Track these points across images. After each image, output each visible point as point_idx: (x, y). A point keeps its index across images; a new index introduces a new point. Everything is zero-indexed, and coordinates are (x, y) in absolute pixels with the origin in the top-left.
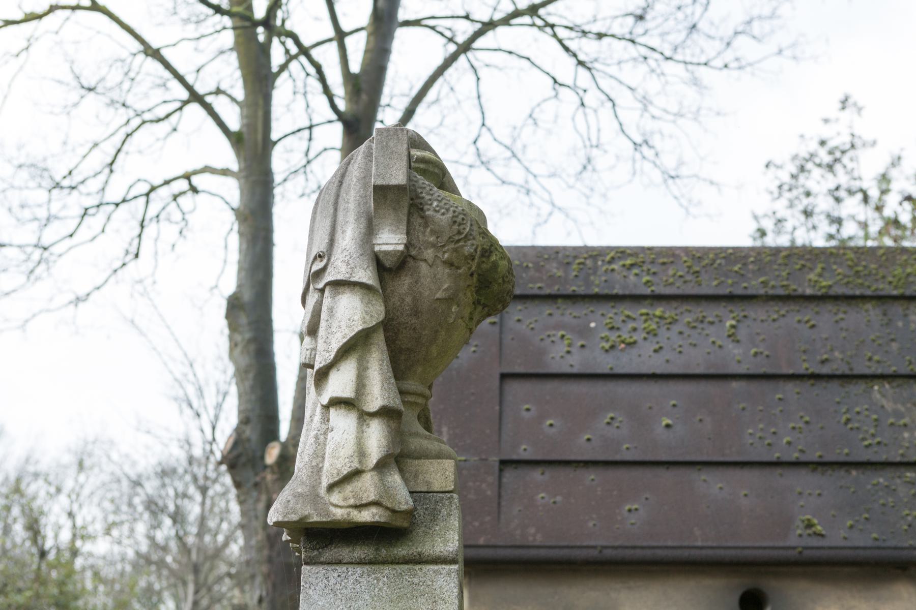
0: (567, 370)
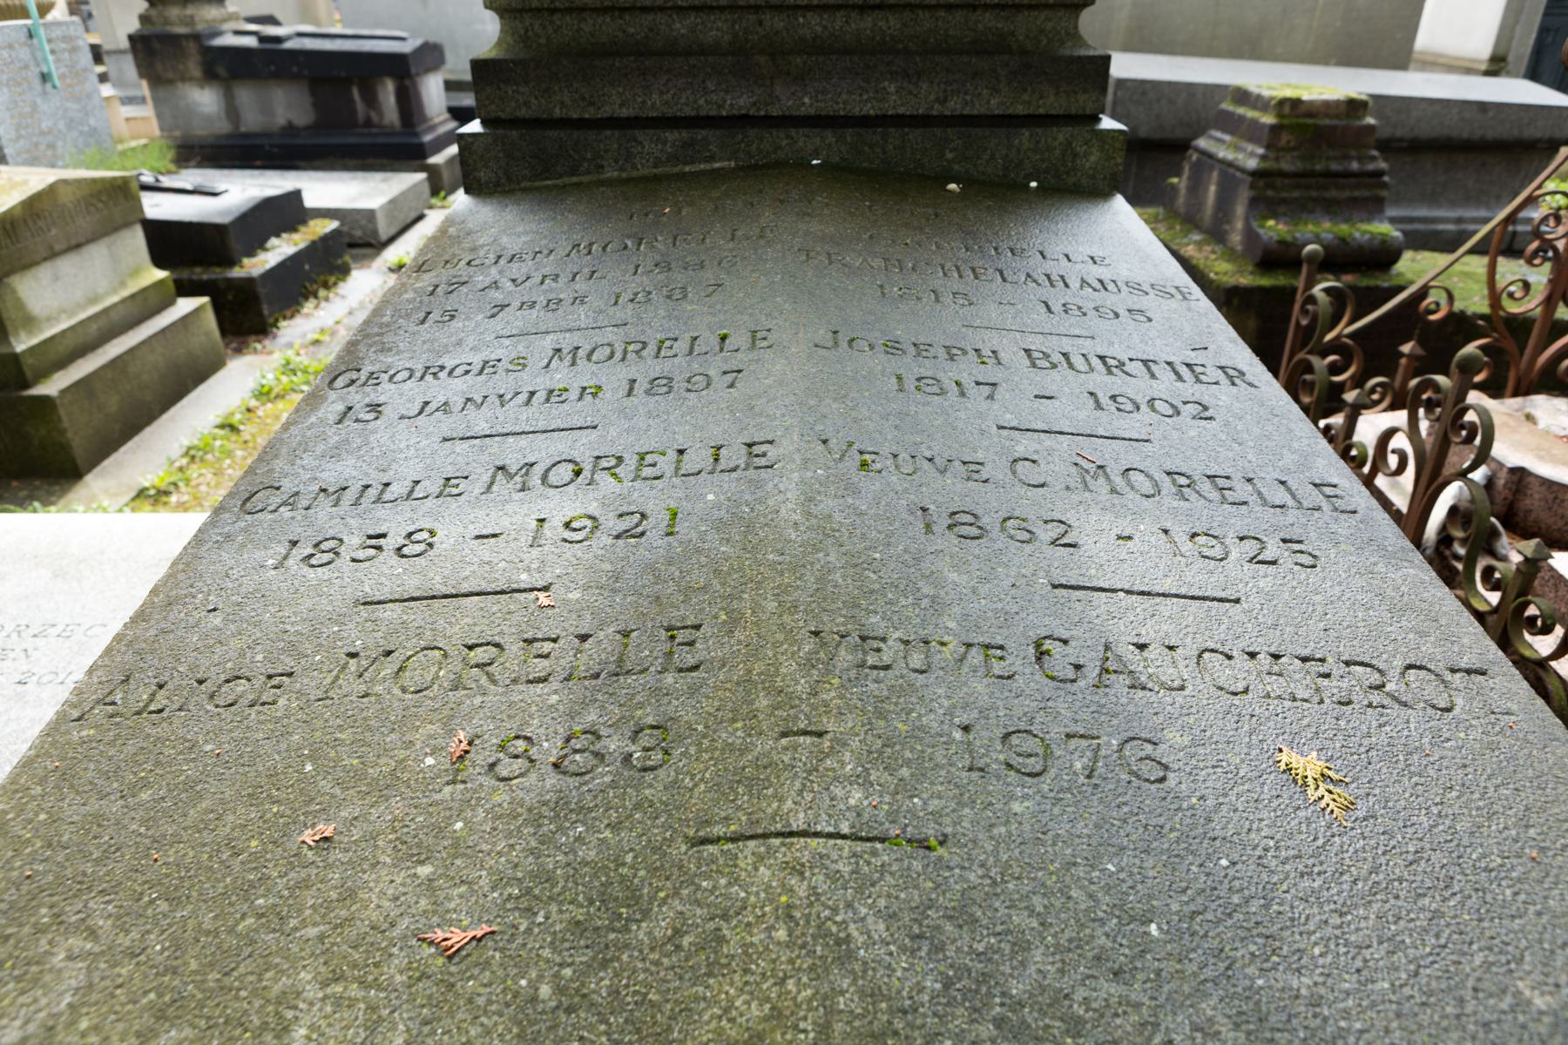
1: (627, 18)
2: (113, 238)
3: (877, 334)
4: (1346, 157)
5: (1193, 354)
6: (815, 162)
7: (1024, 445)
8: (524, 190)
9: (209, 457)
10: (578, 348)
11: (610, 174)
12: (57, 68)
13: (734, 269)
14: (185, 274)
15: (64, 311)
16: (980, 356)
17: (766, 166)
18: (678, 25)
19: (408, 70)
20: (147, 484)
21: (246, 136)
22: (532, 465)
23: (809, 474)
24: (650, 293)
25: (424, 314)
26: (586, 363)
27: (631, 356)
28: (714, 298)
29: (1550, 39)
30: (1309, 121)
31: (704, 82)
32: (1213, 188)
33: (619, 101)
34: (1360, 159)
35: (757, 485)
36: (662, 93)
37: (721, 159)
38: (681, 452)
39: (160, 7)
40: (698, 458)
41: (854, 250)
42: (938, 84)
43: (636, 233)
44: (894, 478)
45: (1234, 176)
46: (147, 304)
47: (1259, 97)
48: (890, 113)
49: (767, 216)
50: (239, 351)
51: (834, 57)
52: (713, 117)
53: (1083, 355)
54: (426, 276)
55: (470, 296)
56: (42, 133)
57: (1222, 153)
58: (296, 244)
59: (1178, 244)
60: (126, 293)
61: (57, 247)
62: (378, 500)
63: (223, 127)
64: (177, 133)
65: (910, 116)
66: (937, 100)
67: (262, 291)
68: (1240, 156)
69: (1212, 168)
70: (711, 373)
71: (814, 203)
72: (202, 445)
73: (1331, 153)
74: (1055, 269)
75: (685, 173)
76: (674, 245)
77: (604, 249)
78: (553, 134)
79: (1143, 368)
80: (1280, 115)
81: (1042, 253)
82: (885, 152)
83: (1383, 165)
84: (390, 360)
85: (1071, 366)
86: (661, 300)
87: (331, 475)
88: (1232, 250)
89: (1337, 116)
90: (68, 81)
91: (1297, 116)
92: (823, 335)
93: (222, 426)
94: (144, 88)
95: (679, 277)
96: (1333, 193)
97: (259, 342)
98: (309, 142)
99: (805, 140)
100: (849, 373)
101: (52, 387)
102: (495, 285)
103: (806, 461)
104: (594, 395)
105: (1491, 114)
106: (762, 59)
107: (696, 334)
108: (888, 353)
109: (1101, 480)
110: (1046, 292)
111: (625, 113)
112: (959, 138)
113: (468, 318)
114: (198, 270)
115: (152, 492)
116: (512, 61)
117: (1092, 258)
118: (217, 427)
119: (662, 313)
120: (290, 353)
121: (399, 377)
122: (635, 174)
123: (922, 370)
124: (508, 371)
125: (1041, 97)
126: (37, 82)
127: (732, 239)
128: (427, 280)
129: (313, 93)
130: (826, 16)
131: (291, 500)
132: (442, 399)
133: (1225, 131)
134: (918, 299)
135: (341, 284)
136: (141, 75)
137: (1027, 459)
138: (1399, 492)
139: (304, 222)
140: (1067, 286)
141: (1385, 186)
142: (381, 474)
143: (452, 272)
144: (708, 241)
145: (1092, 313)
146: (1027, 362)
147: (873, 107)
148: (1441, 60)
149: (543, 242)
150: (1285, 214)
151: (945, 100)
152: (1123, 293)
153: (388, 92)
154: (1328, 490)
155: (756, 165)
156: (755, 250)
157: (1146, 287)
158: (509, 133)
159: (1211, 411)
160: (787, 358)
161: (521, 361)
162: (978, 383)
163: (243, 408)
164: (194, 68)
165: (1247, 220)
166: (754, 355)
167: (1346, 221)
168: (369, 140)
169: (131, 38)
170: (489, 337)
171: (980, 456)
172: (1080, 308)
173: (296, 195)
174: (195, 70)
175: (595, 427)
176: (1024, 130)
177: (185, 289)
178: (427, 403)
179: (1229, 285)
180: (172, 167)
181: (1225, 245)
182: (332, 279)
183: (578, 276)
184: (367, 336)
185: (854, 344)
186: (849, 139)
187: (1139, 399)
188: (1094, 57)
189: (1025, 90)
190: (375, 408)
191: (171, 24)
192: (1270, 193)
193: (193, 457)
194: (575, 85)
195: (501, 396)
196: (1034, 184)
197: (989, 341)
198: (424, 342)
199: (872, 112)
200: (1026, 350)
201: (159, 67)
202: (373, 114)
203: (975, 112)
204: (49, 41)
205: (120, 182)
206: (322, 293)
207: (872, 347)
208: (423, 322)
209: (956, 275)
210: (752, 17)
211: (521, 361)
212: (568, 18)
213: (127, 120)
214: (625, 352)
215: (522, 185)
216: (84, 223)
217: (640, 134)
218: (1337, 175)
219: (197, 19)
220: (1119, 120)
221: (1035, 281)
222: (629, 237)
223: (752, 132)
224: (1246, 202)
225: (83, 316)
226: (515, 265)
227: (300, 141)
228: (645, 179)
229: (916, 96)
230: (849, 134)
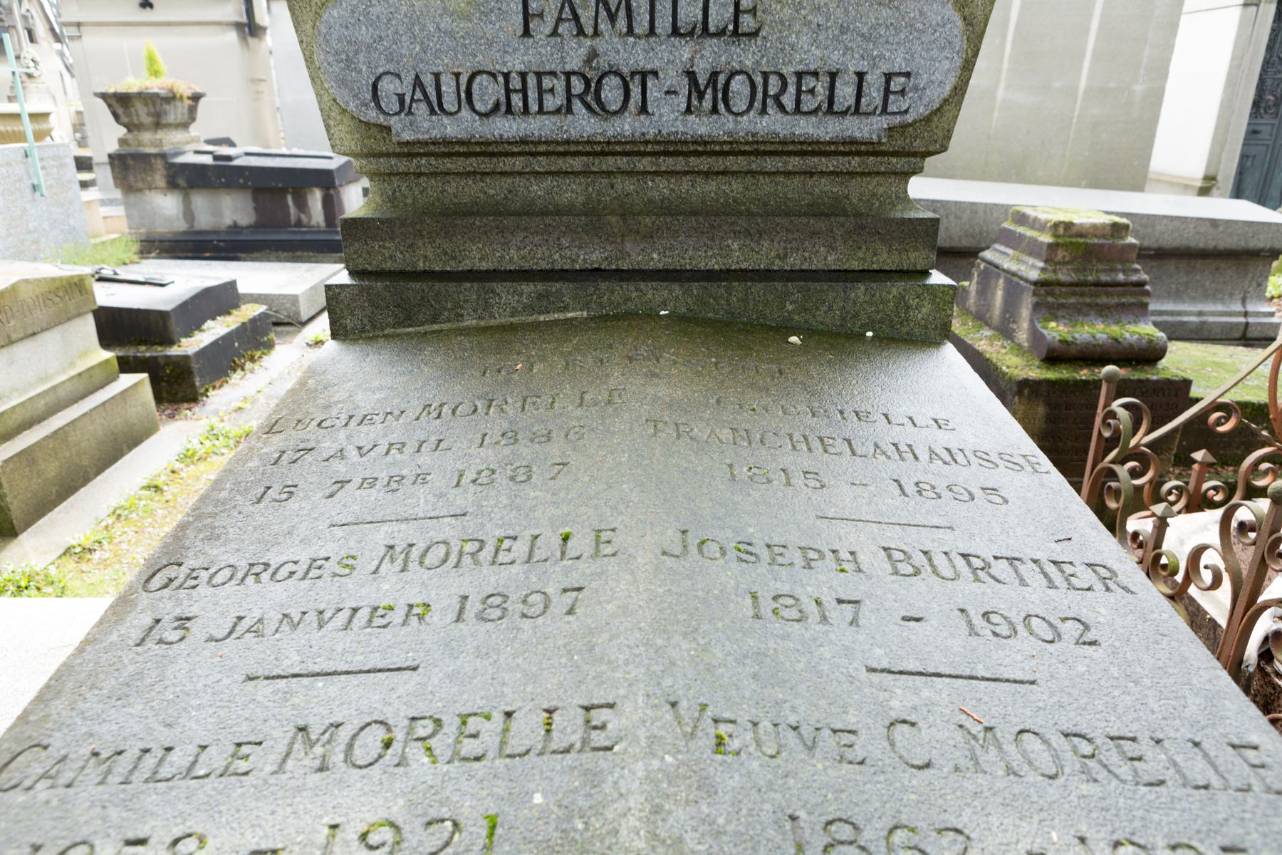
1: (488, 181)
2: (66, 326)
3: (729, 533)
4: (1113, 270)
5: (1058, 547)
6: (662, 313)
7: (902, 695)
8: (386, 337)
9: (134, 516)
10: (411, 545)
11: (470, 322)
12: (45, 181)
13: (581, 443)
14: (130, 352)
15: (17, 390)
16: (838, 560)
17: (616, 317)
18: (535, 188)
19: (334, 182)
20: (74, 543)
21: (199, 233)
22: (338, 726)
23: (656, 764)
24: (493, 472)
25: (263, 489)
26: (418, 568)
27: (467, 560)
28: (559, 482)
29: (1249, 163)
30: (1081, 240)
31: (558, 239)
32: (999, 294)
33: (479, 256)
34: (1124, 272)
35: (593, 778)
36: (519, 248)
37: (574, 310)
38: (509, 715)
39: (136, 133)
40: (527, 730)
41: (701, 419)
42: (779, 243)
43: (487, 394)
44: (755, 764)
45: (1019, 284)
46: (92, 382)
47: (1035, 219)
48: (733, 268)
49: (616, 377)
50: (172, 417)
51: (681, 218)
52: (567, 270)
53: (946, 553)
54: (276, 439)
55: (314, 468)
56: (29, 232)
57: (1007, 264)
58: (228, 326)
59: (972, 339)
60: (74, 372)
61: (14, 336)
62: (154, 778)
63: (181, 226)
64: (143, 230)
65: (752, 271)
66: (778, 256)
67: (195, 366)
68: (1023, 268)
69: (998, 276)
70: (550, 590)
71: (662, 360)
72: (127, 505)
73: (1100, 267)
74: (904, 435)
75: (540, 322)
76: (523, 409)
77: (454, 412)
78: (416, 286)
79: (1010, 570)
80: (1056, 236)
81: (886, 416)
82: (729, 305)
83: (1145, 277)
84: (215, 552)
85: (935, 571)
86: (504, 482)
87: (107, 736)
88: (1020, 345)
89: (1104, 236)
90: (54, 190)
91: (1070, 236)
92: (671, 537)
93: (148, 487)
94: (118, 194)
95: (525, 451)
96: (1104, 300)
97: (190, 409)
98: (250, 238)
99: (653, 293)
100: (700, 593)
101: (290, 199)
102: (341, 455)
103: (652, 739)
104: (421, 617)
105: (1221, 229)
106: (613, 219)
107: (537, 532)
108: (742, 560)
109: (993, 751)
110: (895, 467)
111: (484, 266)
112: (798, 292)
113: (306, 498)
114: (143, 348)
115: (78, 550)
116: (379, 220)
117: (936, 421)
118: (144, 488)
119: (504, 500)
120: (215, 420)
121: (219, 579)
122: (492, 322)
123: (779, 585)
124: (335, 575)
125: (875, 254)
126: (28, 191)
127: (581, 405)
128: (277, 441)
129: (255, 200)
130: (673, 181)
131: (53, 772)
132: (257, 614)
133: (1007, 245)
134: (769, 481)
135: (265, 357)
136: (117, 185)
137: (904, 722)
138: (1218, 605)
139: (237, 306)
140: (916, 458)
141: (1147, 294)
142: (166, 731)
143: (302, 435)
144: (556, 405)
145: (946, 494)
146: (888, 567)
147: (717, 263)
148: (1163, 178)
149: (397, 401)
150: (1064, 317)
151: (785, 256)
152: (973, 466)
153: (316, 199)
154: (1251, 754)
155: (607, 315)
156: (603, 418)
157: (994, 458)
158: (373, 284)
159: (1093, 631)
160: (632, 573)
161: (350, 562)
162: (840, 601)
163: (168, 470)
164: (159, 179)
165: (1032, 321)
166: (595, 566)
167: (1117, 323)
168: (299, 237)
169: (110, 156)
170: (323, 525)
171: (851, 720)
172: (933, 487)
173: (232, 284)
174: (161, 182)
175: (415, 669)
176: (860, 285)
177: (126, 366)
178: (240, 618)
179: (1020, 378)
180: (136, 258)
181: (1013, 341)
182: (258, 354)
183: (424, 445)
184: (199, 517)
185: (704, 547)
186: (695, 292)
187: (1012, 615)
188: (923, 219)
189: (860, 248)
190: (183, 621)
191: (143, 146)
192: (1050, 299)
193: (119, 516)
194: (438, 241)
195: (321, 613)
196: (870, 334)
197: (847, 538)
198: (255, 529)
199: (716, 267)
200: (885, 549)
201: (131, 178)
202: (303, 216)
203: (814, 267)
204: (42, 159)
205: (76, 280)
206: (248, 365)
207: (723, 552)
208: (259, 501)
209: (805, 448)
210: (605, 181)
211: (350, 562)
212: (433, 181)
213: (105, 218)
214: (461, 554)
215: (386, 332)
216: (41, 315)
217: (498, 287)
218: (1107, 285)
219: (164, 141)
220: (951, 278)
221: (884, 453)
222: (479, 398)
223: (604, 286)
224: (1030, 306)
225: (32, 393)
226: (364, 428)
227: (242, 238)
228: (502, 328)
229: (757, 253)
230: (695, 287)
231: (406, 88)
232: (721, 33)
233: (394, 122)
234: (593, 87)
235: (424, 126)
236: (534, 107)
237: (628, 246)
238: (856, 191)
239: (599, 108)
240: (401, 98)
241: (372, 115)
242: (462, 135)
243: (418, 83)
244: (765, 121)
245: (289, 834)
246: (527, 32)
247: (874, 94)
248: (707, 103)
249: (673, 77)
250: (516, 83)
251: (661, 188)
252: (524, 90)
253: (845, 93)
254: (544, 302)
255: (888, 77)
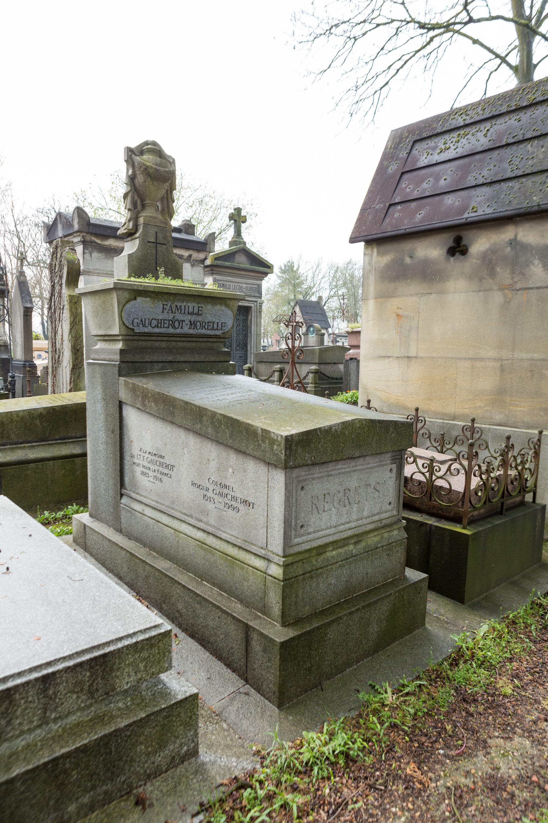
0: (424, 165)
78: (138, 364)
111: (149, 360)
231: (139, 321)
232: (196, 314)
233: (135, 328)
234: (173, 323)
235: (141, 329)
236: (162, 326)
237: (177, 356)
238: (215, 345)
239: (174, 327)
240: (138, 323)
241: (131, 327)
242: (148, 331)
243: (142, 320)
244: (202, 331)
245: (218, 419)
246: (163, 312)
247: (220, 326)
248: (193, 327)
249: (187, 322)
250: (160, 321)
251: (180, 344)
252: (161, 323)
253: (215, 326)
254: (163, 368)
255: (222, 323)
